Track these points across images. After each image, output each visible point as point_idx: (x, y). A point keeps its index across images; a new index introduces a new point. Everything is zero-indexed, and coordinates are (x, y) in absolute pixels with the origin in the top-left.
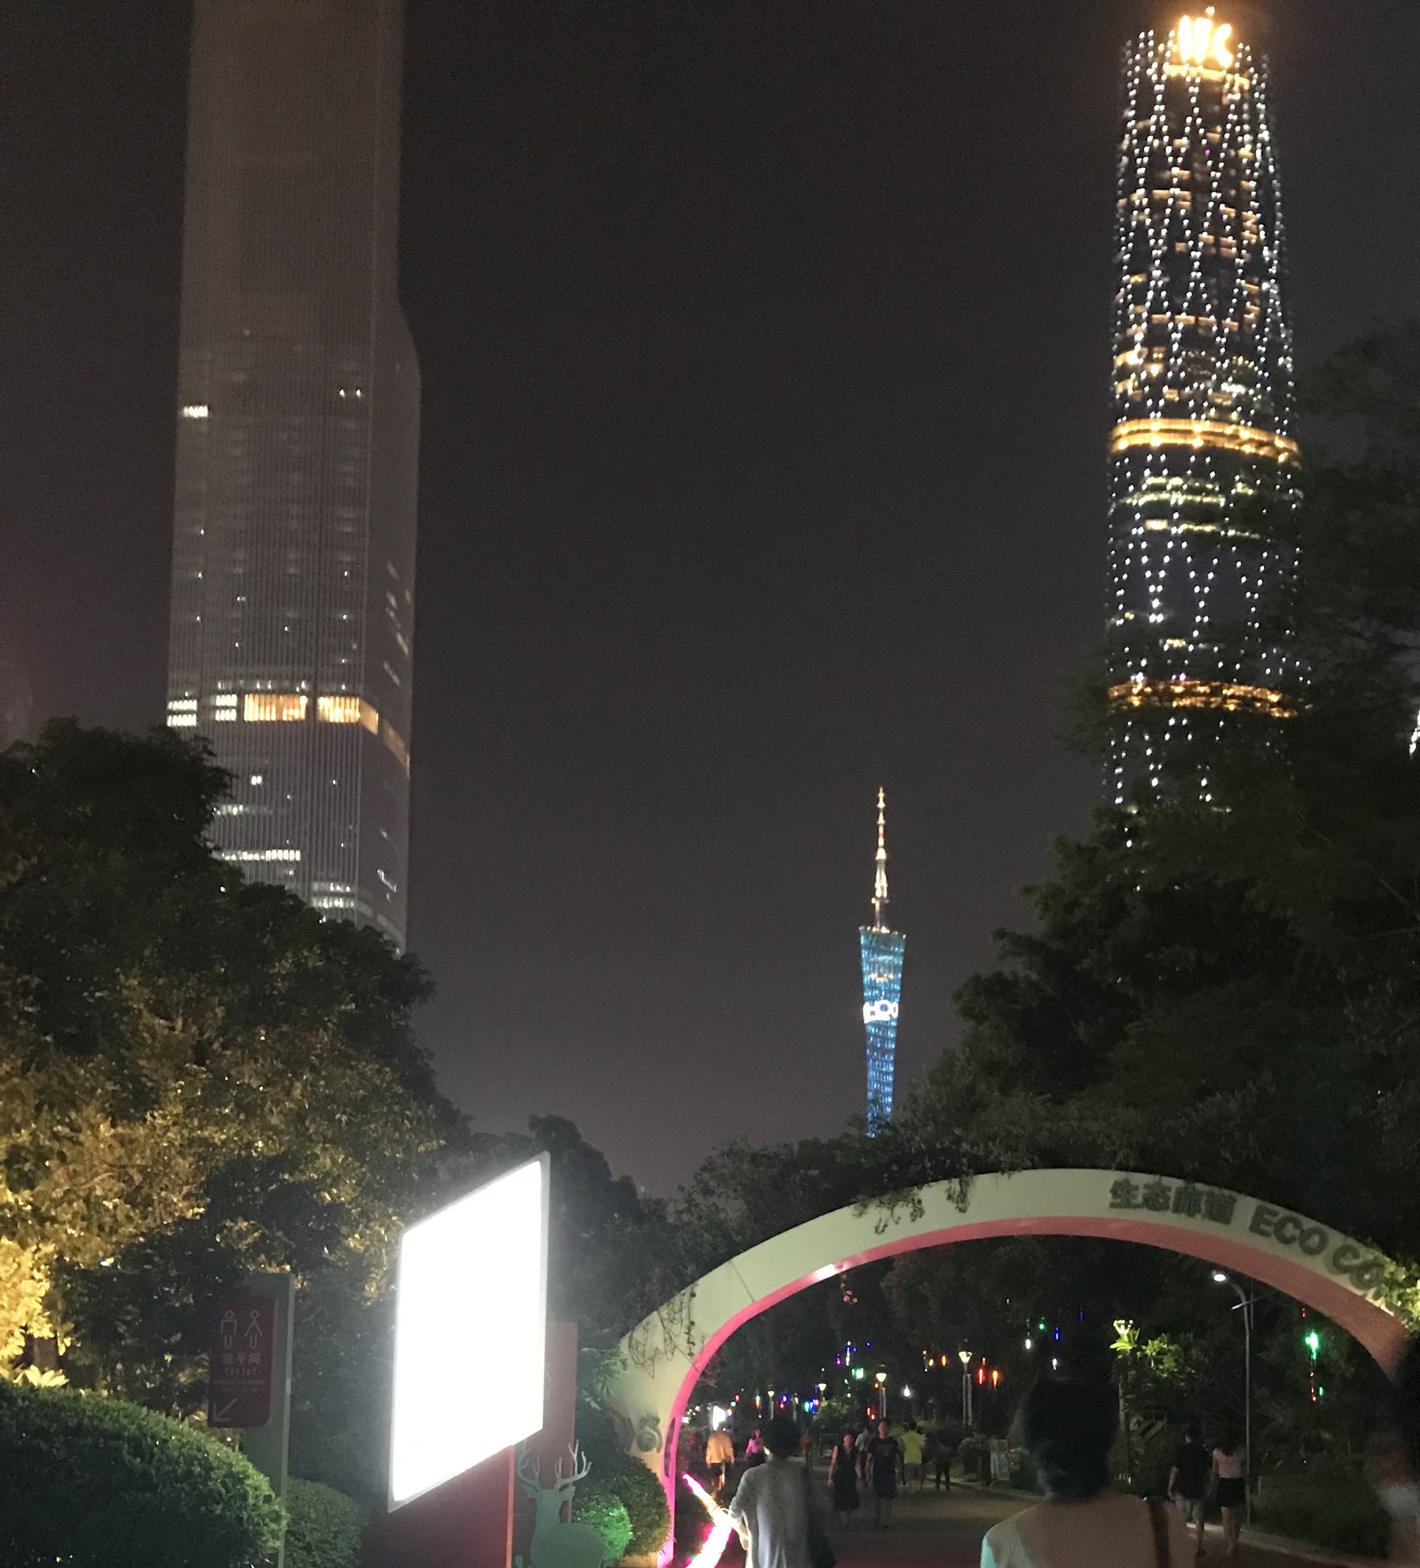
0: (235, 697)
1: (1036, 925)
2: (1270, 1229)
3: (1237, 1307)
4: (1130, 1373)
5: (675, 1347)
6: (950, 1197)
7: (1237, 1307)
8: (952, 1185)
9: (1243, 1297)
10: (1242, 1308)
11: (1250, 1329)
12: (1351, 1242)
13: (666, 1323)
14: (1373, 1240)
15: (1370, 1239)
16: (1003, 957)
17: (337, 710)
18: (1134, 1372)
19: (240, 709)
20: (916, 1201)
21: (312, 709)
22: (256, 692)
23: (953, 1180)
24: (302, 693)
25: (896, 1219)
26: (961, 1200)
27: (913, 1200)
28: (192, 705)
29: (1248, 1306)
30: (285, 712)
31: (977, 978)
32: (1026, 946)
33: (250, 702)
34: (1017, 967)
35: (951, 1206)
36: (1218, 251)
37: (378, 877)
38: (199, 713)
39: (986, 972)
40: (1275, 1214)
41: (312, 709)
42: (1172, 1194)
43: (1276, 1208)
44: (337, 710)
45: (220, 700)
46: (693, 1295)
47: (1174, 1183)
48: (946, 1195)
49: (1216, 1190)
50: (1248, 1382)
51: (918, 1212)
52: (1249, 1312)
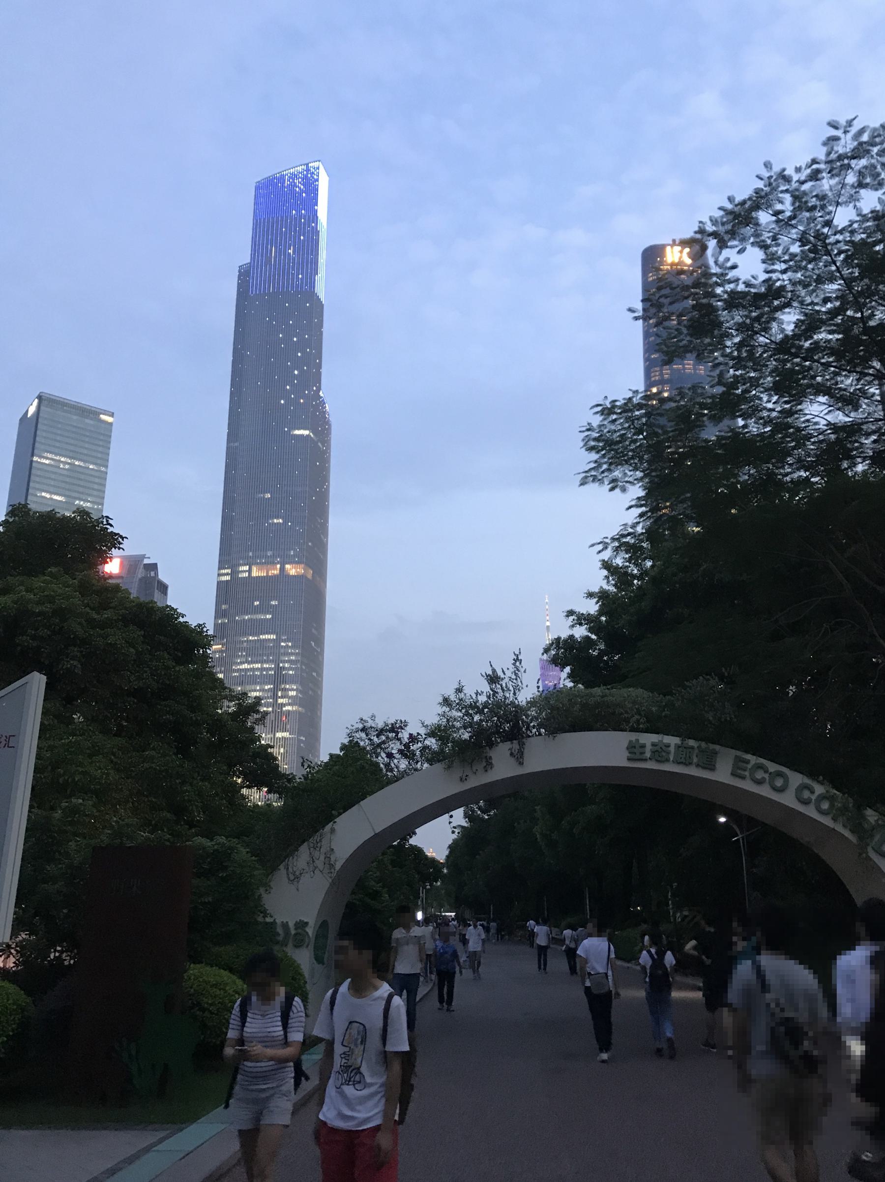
0: (248, 567)
1: (592, 607)
2: (747, 773)
3: (736, 838)
4: (674, 884)
5: (316, 868)
6: (512, 754)
7: (736, 838)
8: (514, 745)
9: (739, 832)
10: (738, 840)
11: (745, 853)
12: (807, 781)
13: (312, 849)
14: (824, 779)
15: (821, 778)
16: (573, 626)
17: (292, 570)
18: (676, 884)
19: (250, 571)
20: (488, 758)
21: (282, 569)
22: (258, 564)
23: (514, 741)
24: (278, 563)
25: (474, 771)
26: (519, 757)
27: (486, 757)
28: (229, 571)
29: (743, 838)
30: (270, 572)
31: (559, 639)
32: (582, 619)
33: (254, 569)
34: (580, 632)
35: (512, 761)
36: (684, 371)
37: (311, 644)
38: (231, 574)
39: (564, 635)
40: (748, 762)
41: (282, 569)
42: (672, 749)
43: (748, 757)
44: (292, 570)
45: (242, 568)
46: (333, 831)
47: (673, 741)
48: (509, 752)
49: (703, 745)
50: (746, 892)
51: (489, 765)
52: (743, 843)
